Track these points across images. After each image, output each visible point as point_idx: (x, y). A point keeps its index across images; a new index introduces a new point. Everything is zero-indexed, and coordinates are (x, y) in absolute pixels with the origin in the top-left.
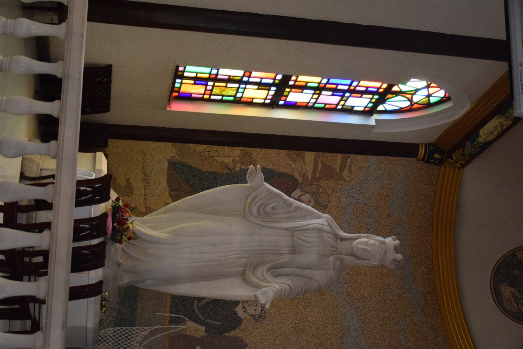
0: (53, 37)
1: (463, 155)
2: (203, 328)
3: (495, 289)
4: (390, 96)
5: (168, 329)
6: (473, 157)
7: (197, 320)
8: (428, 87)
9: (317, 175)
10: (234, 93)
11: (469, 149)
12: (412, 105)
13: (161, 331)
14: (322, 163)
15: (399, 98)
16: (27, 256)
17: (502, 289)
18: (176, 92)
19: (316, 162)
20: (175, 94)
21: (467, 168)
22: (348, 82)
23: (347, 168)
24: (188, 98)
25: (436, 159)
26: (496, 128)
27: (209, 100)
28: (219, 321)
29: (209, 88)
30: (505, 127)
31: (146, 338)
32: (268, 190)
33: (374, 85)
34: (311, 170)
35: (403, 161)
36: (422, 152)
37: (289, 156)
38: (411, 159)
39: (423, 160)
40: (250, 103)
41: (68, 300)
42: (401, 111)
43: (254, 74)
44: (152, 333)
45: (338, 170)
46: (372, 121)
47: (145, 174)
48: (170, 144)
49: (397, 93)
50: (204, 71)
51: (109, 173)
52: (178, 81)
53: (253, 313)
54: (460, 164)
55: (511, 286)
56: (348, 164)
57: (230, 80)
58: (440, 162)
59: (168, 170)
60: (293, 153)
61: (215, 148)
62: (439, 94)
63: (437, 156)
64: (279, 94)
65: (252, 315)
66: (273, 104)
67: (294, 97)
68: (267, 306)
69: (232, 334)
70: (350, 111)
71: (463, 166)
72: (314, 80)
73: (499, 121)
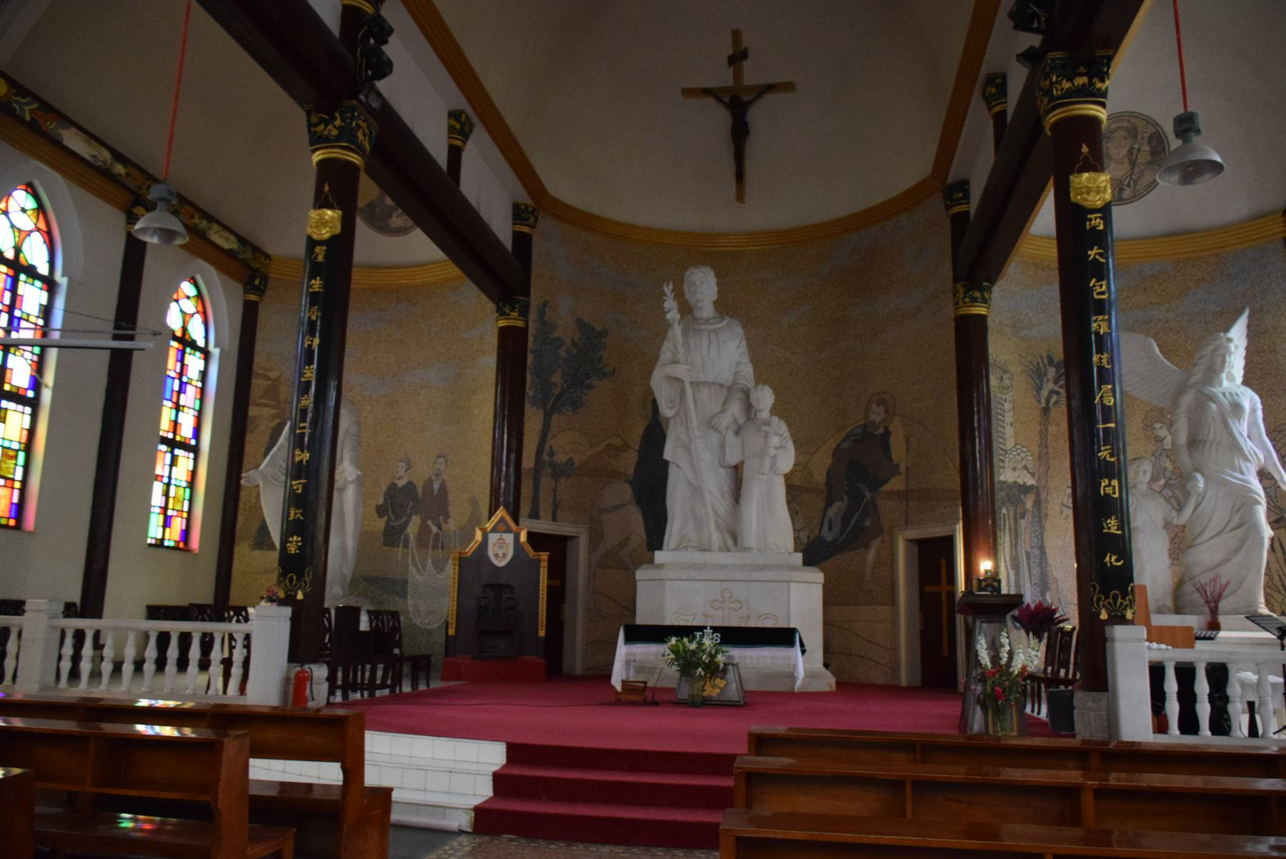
0: (143, 676)
1: (254, 259)
2: (414, 517)
3: (394, 232)
4: (187, 337)
5: (413, 549)
6: (257, 250)
7: (407, 522)
8: (177, 301)
9: (274, 403)
10: (182, 490)
11: (248, 255)
12: (198, 312)
13: (413, 556)
14: (261, 399)
15: (190, 327)
16: (407, 694)
17: (394, 226)
18: (178, 544)
19: (260, 405)
20: (181, 545)
21: (270, 253)
22: (169, 381)
23: (267, 373)
24: (186, 534)
25: (260, 283)
26: (221, 236)
27: (189, 512)
28: (408, 503)
29: (175, 513)
30: (220, 228)
31: (418, 571)
32: (266, 465)
33: (172, 355)
34: (269, 409)
35: (262, 316)
36: (253, 297)
37: (252, 431)
38: (260, 308)
39: (260, 296)
40: (194, 473)
41: (1192, 650)
42: (206, 323)
43: (158, 471)
44: (415, 565)
45: (270, 382)
46: (215, 352)
47: (266, 572)
48: (236, 549)
49: (184, 329)
50: (156, 521)
51: (651, 553)
52: (166, 543)
53: (404, 470)
54: (265, 259)
55: (390, 216)
56: (263, 372)
57: (166, 494)
58: (265, 279)
59: (263, 550)
60: (249, 428)
61: (241, 505)
62: (187, 288)
63: (257, 282)
64: (184, 446)
65: (406, 471)
66: (195, 450)
67: (186, 431)
68: (359, 473)
69: (420, 491)
70: (204, 375)
71: (268, 256)
72: (167, 414)
73: (214, 236)
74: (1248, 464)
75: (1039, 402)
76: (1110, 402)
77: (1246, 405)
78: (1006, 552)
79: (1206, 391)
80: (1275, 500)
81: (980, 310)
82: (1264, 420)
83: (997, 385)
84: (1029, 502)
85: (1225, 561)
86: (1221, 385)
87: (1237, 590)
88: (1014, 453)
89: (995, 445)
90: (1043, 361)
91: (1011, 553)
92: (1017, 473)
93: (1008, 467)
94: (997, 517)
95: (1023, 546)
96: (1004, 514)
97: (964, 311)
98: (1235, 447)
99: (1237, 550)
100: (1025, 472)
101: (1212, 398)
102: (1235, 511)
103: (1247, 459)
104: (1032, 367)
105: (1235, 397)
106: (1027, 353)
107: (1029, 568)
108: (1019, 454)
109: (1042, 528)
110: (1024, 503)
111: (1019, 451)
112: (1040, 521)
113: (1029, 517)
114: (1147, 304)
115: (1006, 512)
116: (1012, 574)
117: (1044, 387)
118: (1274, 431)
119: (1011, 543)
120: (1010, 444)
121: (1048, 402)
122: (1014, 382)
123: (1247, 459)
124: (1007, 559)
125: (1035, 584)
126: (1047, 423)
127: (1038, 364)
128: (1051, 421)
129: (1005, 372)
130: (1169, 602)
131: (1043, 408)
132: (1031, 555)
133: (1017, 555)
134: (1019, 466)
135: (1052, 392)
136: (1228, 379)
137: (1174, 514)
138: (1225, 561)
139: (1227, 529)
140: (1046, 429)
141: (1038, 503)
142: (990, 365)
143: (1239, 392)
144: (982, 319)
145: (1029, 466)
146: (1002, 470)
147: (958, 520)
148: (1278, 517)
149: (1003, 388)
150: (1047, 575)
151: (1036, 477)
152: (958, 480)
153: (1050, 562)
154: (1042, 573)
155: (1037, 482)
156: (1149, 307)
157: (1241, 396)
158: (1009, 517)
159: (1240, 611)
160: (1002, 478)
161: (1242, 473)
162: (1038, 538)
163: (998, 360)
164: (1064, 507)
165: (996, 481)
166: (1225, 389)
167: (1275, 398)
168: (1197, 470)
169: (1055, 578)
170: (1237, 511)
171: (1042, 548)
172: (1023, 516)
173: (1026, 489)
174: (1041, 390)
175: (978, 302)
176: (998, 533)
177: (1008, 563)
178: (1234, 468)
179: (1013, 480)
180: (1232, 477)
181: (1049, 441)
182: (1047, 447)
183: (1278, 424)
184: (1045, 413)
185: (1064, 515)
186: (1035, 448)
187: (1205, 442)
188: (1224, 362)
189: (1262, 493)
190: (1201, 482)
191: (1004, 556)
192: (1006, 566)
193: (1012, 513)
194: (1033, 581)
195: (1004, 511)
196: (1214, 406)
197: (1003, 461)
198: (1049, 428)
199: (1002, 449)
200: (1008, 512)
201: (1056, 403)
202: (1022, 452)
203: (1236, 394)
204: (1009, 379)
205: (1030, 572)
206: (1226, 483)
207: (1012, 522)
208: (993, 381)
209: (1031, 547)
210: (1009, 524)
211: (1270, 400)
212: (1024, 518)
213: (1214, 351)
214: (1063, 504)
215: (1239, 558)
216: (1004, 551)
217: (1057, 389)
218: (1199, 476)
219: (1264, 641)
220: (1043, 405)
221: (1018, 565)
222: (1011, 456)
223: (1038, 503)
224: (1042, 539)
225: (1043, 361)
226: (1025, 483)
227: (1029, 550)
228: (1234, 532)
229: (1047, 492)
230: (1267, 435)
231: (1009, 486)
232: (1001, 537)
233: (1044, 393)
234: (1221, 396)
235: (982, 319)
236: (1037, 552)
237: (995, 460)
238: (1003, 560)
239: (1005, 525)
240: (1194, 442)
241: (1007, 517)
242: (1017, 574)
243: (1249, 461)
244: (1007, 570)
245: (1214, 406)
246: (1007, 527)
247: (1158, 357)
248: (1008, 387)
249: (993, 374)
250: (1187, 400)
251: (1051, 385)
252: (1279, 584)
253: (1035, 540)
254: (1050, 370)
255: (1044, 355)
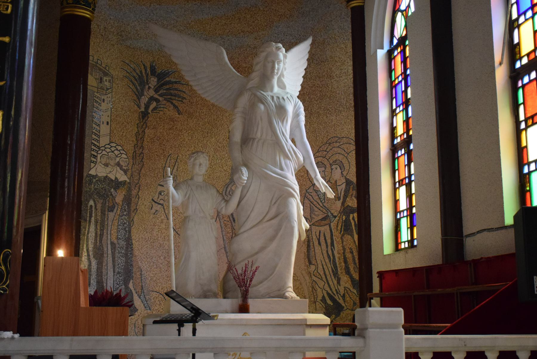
74: (288, 161)
75: (139, 107)
76: (7, 9)
77: (290, 109)
78: (90, 242)
79: (258, 94)
80: (323, 202)
81: (85, 13)
82: (305, 126)
83: (96, 85)
84: (119, 197)
85: (263, 249)
86: (272, 90)
87: (271, 275)
88: (108, 150)
89: (87, 140)
90: (146, 70)
91: (95, 244)
92: (109, 169)
93: (100, 162)
94: (83, 208)
95: (109, 237)
96: (91, 206)
97: (68, 11)
98: (277, 144)
99: (272, 239)
100: (118, 168)
101: (262, 100)
102: (273, 203)
103: (287, 157)
104: (135, 75)
105: (281, 100)
106: (131, 61)
107: (114, 258)
108: (113, 152)
109: (131, 222)
110: (114, 198)
111: (113, 149)
112: (129, 214)
113: (118, 210)
114: (240, 31)
115: (93, 205)
116: (94, 263)
117: (145, 93)
118: (326, 143)
119: (96, 234)
120: (104, 141)
121: (147, 106)
122: (114, 85)
123: (287, 157)
124: (90, 249)
125: (119, 273)
126: (144, 126)
127: (141, 72)
128: (148, 125)
129: (106, 74)
130: (216, 287)
131: (142, 112)
132: (117, 246)
133: (101, 245)
134: (112, 163)
135: (152, 99)
136: (279, 86)
137: (223, 204)
138: (263, 249)
139: (267, 218)
140: (143, 131)
141: (128, 200)
142: (90, 65)
143: (285, 97)
144: (87, 22)
145: (122, 163)
146: (93, 165)
147: (46, 210)
148: (326, 215)
149: (102, 88)
150: (132, 265)
151: (129, 173)
152: (49, 172)
153: (136, 252)
154: (126, 262)
155: (130, 179)
156: (242, 34)
157: (286, 100)
158: (96, 209)
159: (272, 295)
160: (92, 172)
161: (282, 169)
162: (126, 231)
163: (99, 62)
164: (153, 203)
165: (85, 174)
166: (275, 94)
167: (328, 116)
168: (246, 165)
169: (139, 267)
170: (275, 203)
171: (129, 241)
172: (111, 209)
173: (117, 184)
174: (141, 96)
175: (81, 4)
176: (83, 224)
177: (91, 253)
178: (275, 165)
179: (105, 175)
180: (272, 172)
181: (145, 143)
182: (142, 147)
183: (329, 137)
184: (143, 117)
185: (153, 211)
186: (130, 147)
187: (254, 139)
188: (273, 68)
189: (297, 187)
190: (245, 174)
191: (87, 245)
192: (88, 255)
193: (99, 206)
194: (117, 270)
195: (91, 203)
196: (262, 107)
197: (95, 157)
198: (147, 131)
199: (95, 145)
200: (95, 203)
201: (155, 109)
202: (117, 150)
203: (283, 98)
204: (109, 81)
205: (114, 261)
206: (267, 177)
207: (99, 214)
208: (92, 81)
209: (118, 238)
210: (96, 215)
211: (325, 118)
212: (112, 211)
213: (266, 57)
214: (153, 200)
215: (274, 245)
216: (87, 241)
217: (156, 96)
218: (244, 170)
219: (282, 322)
220: (143, 109)
221: (102, 255)
222: (104, 152)
223: (128, 200)
224: (130, 232)
225: (146, 70)
226: (116, 178)
227: (115, 241)
228: (273, 221)
229: (139, 189)
230: (307, 138)
231: (99, 180)
232: (85, 228)
233: (144, 100)
234: (269, 98)
235: (87, 22)
236: (123, 243)
237: (87, 155)
238: (85, 250)
239: (91, 216)
240: (246, 140)
241: (93, 209)
242: (100, 264)
243: (289, 159)
244: (89, 259)
245: (262, 107)
246: (93, 218)
247: (226, 63)
248: (108, 89)
249: (92, 75)
250: (243, 101)
251: (152, 93)
252: (322, 273)
253: (123, 232)
254: (152, 79)
255: (148, 65)
